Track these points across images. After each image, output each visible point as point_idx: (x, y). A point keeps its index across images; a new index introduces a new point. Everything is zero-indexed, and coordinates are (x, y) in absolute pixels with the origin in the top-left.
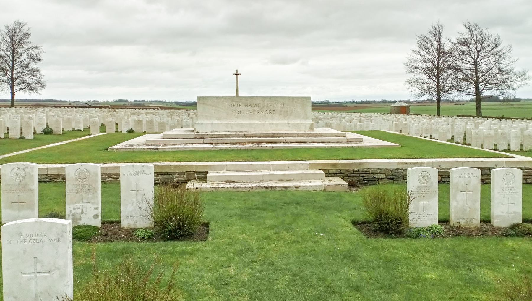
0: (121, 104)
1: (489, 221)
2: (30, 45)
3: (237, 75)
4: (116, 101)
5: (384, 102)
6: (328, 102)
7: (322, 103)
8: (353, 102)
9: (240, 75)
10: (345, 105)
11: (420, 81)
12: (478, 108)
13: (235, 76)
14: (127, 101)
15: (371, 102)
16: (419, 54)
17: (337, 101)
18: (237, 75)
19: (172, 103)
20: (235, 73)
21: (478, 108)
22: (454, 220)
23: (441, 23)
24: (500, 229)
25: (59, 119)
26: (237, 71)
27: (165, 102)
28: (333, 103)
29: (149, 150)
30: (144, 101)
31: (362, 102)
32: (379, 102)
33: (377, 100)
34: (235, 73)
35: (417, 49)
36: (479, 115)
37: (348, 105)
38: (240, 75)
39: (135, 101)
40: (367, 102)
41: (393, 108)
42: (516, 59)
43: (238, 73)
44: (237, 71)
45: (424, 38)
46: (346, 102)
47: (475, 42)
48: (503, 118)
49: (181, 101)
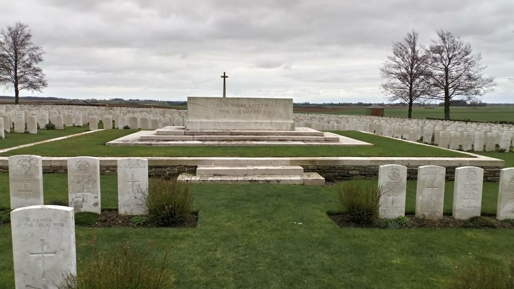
0: (118, 102)
3: (224, 77)
9: (227, 77)
10: (324, 107)
13: (223, 78)
14: (122, 100)
18: (224, 77)
19: (164, 102)
20: (223, 75)
23: (416, 31)
26: (224, 73)
28: (313, 104)
31: (340, 105)
32: (355, 105)
33: (353, 103)
35: (393, 55)
38: (227, 77)
39: (130, 100)
41: (369, 110)
42: (484, 66)
43: (226, 75)
44: (224, 73)
46: (325, 104)
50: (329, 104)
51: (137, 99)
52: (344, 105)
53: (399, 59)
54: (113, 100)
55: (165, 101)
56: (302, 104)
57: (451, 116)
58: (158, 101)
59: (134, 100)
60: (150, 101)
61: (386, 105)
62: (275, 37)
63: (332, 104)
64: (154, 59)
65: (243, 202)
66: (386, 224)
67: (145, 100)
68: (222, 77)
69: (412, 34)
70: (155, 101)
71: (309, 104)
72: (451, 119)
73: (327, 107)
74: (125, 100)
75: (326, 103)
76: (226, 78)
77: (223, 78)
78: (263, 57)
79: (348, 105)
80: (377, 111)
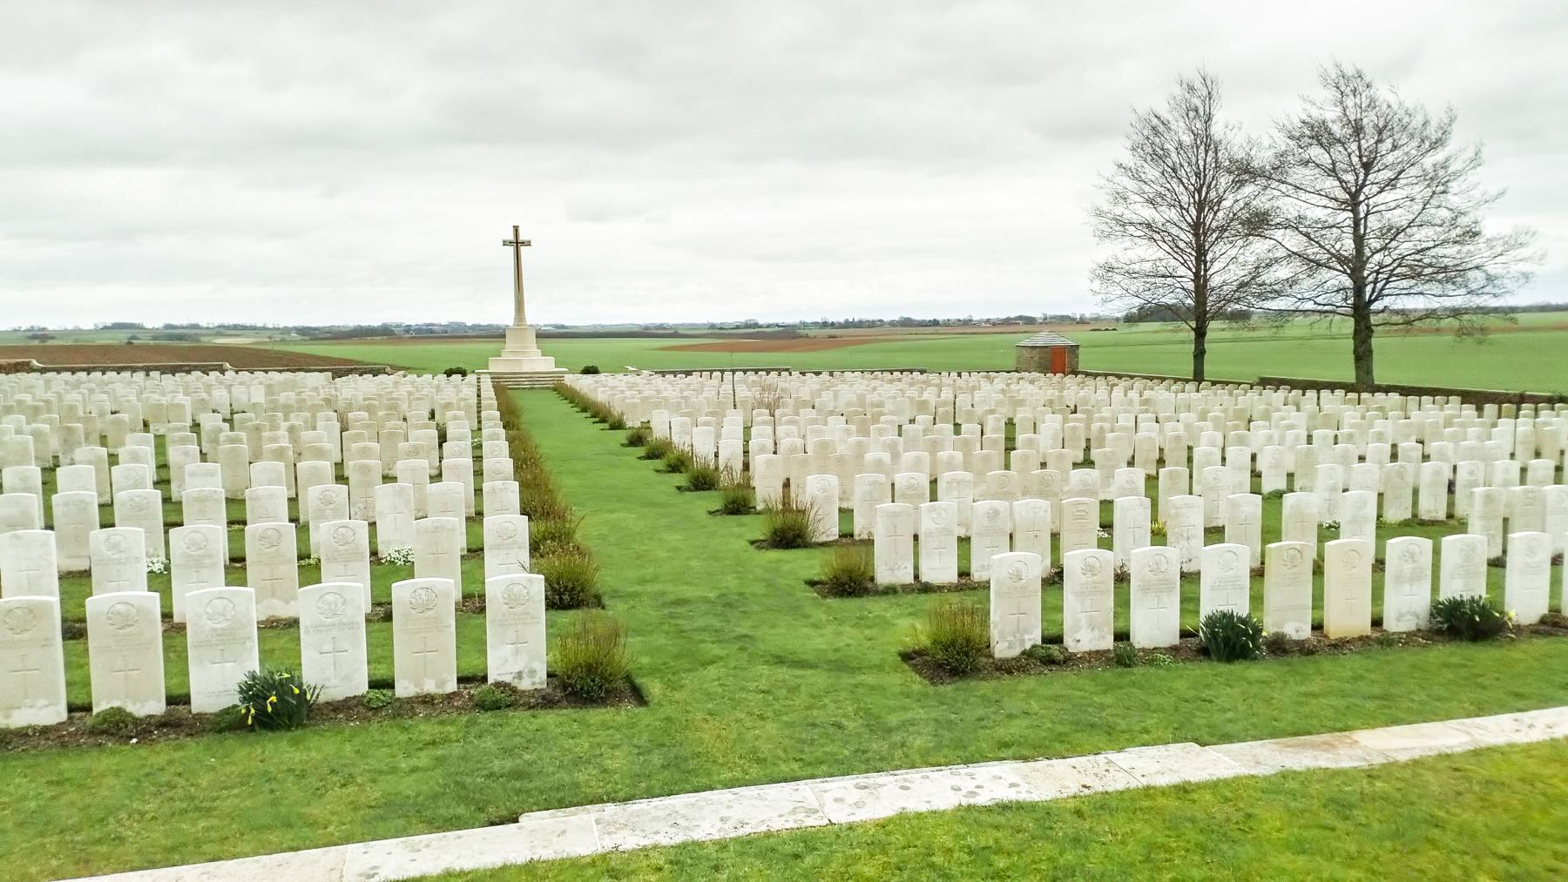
1: (968, 575)
3: (517, 244)
4: (106, 328)
5: (907, 323)
6: (756, 325)
7: (738, 327)
8: (825, 325)
9: (528, 244)
10: (803, 332)
11: (1136, 267)
15: (872, 324)
17: (780, 322)
18: (517, 244)
19: (286, 330)
20: (511, 237)
22: (924, 579)
23: (1211, 73)
25: (305, 604)
26: (516, 229)
27: (264, 328)
28: (769, 326)
30: (196, 326)
31: (848, 325)
32: (892, 324)
33: (887, 319)
34: (511, 237)
35: (1129, 159)
36: (1363, 383)
37: (812, 332)
38: (528, 244)
40: (860, 324)
41: (1027, 354)
44: (516, 229)
45: (1155, 121)
46: (805, 325)
47: (1358, 146)
48: (1521, 399)
49: (314, 325)
53: (1152, 172)
55: (290, 325)
57: (1380, 376)
60: (661, 327)
61: (981, 322)
65: (104, 849)
69: (1198, 84)
72: (1499, 553)
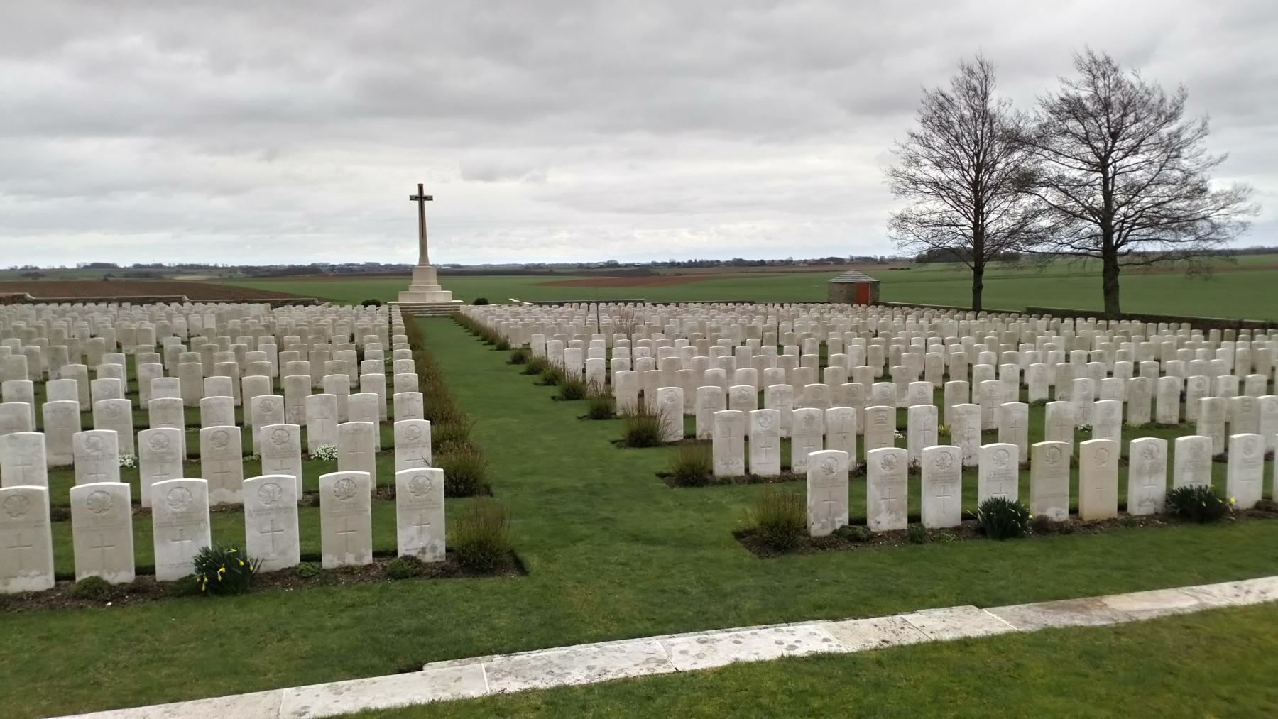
2: (1066, 87)
3: (421, 198)
7: (601, 267)
9: (430, 198)
12: (1111, 290)
13: (416, 203)
16: (926, 143)
18: (421, 198)
19: (233, 269)
20: (416, 193)
21: (1111, 290)
23: (987, 58)
24: (820, 538)
25: (249, 493)
26: (421, 187)
28: (627, 265)
29: (29, 279)
31: (691, 265)
32: (727, 264)
33: (723, 259)
34: (416, 193)
35: (919, 129)
38: (430, 198)
39: (137, 266)
41: (837, 288)
42: (1217, 154)
43: (426, 193)
44: (421, 187)
46: (655, 265)
50: (665, 264)
51: (157, 262)
52: (702, 264)
53: (939, 141)
54: (86, 267)
56: (601, 266)
58: (216, 268)
59: (148, 267)
62: (499, 113)
63: (672, 264)
64: (192, 160)
66: (726, 481)
67: (180, 266)
68: (412, 198)
69: (976, 68)
70: (207, 268)
71: (616, 265)
73: (661, 272)
74: (122, 266)
75: (659, 261)
76: (426, 203)
77: (416, 203)
78: (480, 155)
79: (710, 264)
80: (858, 285)
